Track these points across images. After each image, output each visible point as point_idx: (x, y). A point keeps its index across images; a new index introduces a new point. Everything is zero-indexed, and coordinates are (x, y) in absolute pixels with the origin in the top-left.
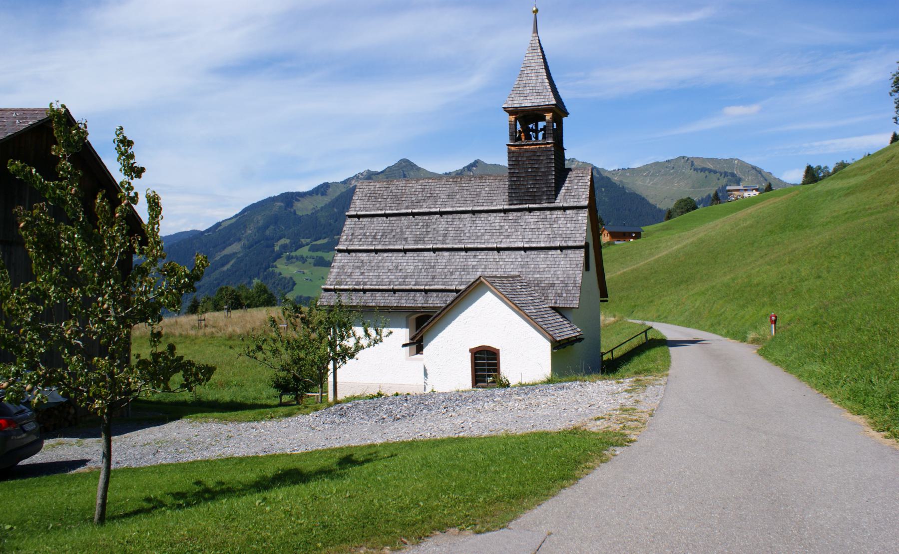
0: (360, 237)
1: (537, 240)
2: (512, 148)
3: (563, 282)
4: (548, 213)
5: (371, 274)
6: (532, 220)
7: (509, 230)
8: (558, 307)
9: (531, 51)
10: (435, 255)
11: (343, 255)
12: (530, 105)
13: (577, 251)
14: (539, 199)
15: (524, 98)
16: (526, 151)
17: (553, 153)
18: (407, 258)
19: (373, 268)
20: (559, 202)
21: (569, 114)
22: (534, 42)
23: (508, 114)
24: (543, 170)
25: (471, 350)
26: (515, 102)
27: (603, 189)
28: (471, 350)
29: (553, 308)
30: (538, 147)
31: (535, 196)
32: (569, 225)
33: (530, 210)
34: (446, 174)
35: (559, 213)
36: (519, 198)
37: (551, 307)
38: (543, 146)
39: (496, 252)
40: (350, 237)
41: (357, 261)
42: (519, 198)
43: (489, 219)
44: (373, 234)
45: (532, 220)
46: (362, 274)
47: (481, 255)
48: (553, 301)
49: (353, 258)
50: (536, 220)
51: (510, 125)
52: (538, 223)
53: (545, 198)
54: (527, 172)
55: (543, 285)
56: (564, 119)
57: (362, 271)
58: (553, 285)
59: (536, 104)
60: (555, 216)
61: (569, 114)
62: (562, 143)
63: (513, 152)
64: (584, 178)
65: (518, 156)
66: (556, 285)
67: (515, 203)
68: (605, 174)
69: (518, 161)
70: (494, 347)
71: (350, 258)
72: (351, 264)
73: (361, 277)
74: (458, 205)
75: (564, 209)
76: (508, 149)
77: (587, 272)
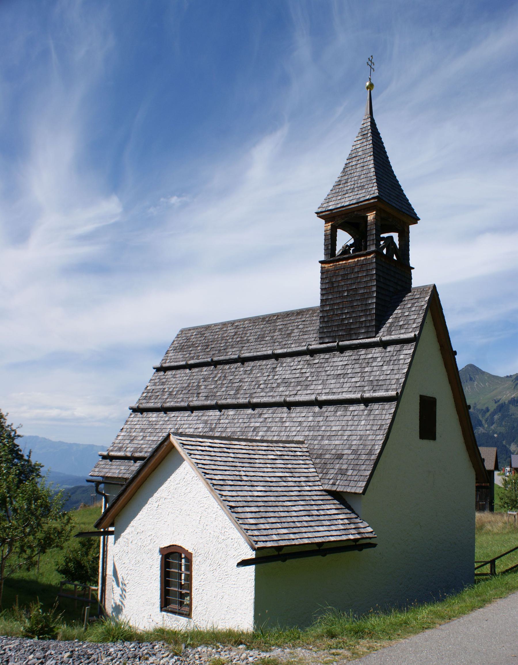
1: (340, 390)
2: (326, 266)
3: (355, 452)
4: (363, 351)
6: (341, 363)
7: (309, 379)
8: (343, 492)
12: (347, 204)
13: (387, 406)
14: (355, 334)
16: (344, 268)
17: (374, 265)
20: (383, 335)
21: (419, 219)
22: (365, 125)
23: (323, 221)
24: (361, 291)
26: (330, 204)
28: (162, 550)
29: (329, 492)
30: (356, 260)
31: (351, 329)
32: (385, 368)
33: (342, 349)
34: (507, 376)
35: (376, 352)
37: (325, 491)
38: (362, 258)
39: (285, 409)
44: (171, 390)
45: (341, 363)
47: (268, 413)
48: (331, 482)
50: (346, 363)
51: (325, 236)
52: (347, 367)
53: (363, 331)
55: (327, 456)
56: (412, 228)
58: (340, 457)
59: (354, 201)
60: (370, 356)
61: (419, 219)
62: (408, 259)
63: (328, 271)
64: (420, 300)
66: (345, 457)
67: (327, 341)
69: (332, 283)
74: (264, 349)
76: (322, 268)
77: (427, 443)
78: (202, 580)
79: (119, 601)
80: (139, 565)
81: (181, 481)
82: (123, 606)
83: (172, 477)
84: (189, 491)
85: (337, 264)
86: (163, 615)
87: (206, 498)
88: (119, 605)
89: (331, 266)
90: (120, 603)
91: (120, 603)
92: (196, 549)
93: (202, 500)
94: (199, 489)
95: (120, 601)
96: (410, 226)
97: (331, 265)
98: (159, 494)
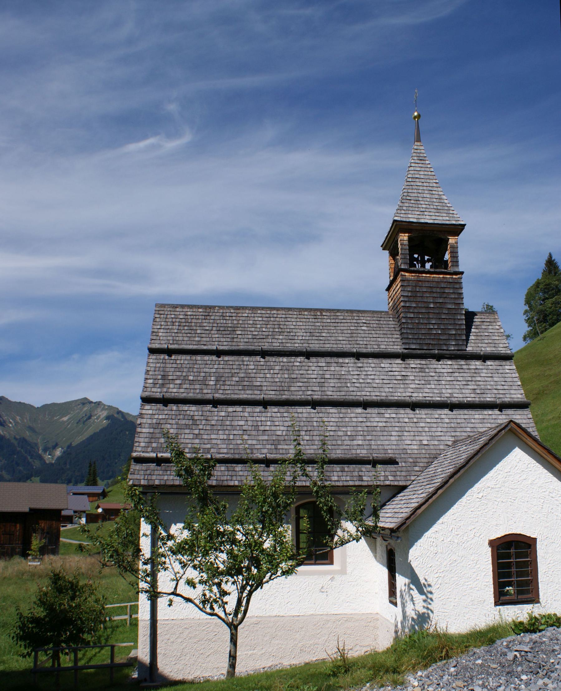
0: (178, 382)
5: (213, 436)
9: (419, 162)
10: (316, 411)
11: (154, 408)
14: (446, 344)
15: (421, 213)
18: (269, 415)
19: (215, 428)
24: (450, 306)
25: (492, 543)
27: (127, 433)
28: (492, 543)
30: (441, 276)
36: (418, 341)
38: (448, 276)
40: (160, 382)
41: (181, 417)
42: (418, 341)
43: (383, 365)
46: (197, 436)
47: (389, 413)
49: (173, 413)
53: (453, 343)
54: (428, 308)
57: (196, 432)
65: (416, 286)
68: (130, 419)
70: (528, 535)
71: (170, 412)
72: (174, 422)
73: (197, 441)
75: (484, 358)
78: (552, 562)
79: (422, 608)
80: (455, 564)
81: (512, 469)
82: (429, 612)
83: (498, 466)
84: (524, 478)
85: (420, 275)
86: (500, 609)
87: (548, 484)
88: (424, 613)
89: (412, 276)
90: (425, 610)
91: (425, 610)
92: (542, 533)
93: (542, 485)
94: (538, 475)
95: (424, 607)
96: (388, 251)
97: (413, 275)
98: (481, 485)
